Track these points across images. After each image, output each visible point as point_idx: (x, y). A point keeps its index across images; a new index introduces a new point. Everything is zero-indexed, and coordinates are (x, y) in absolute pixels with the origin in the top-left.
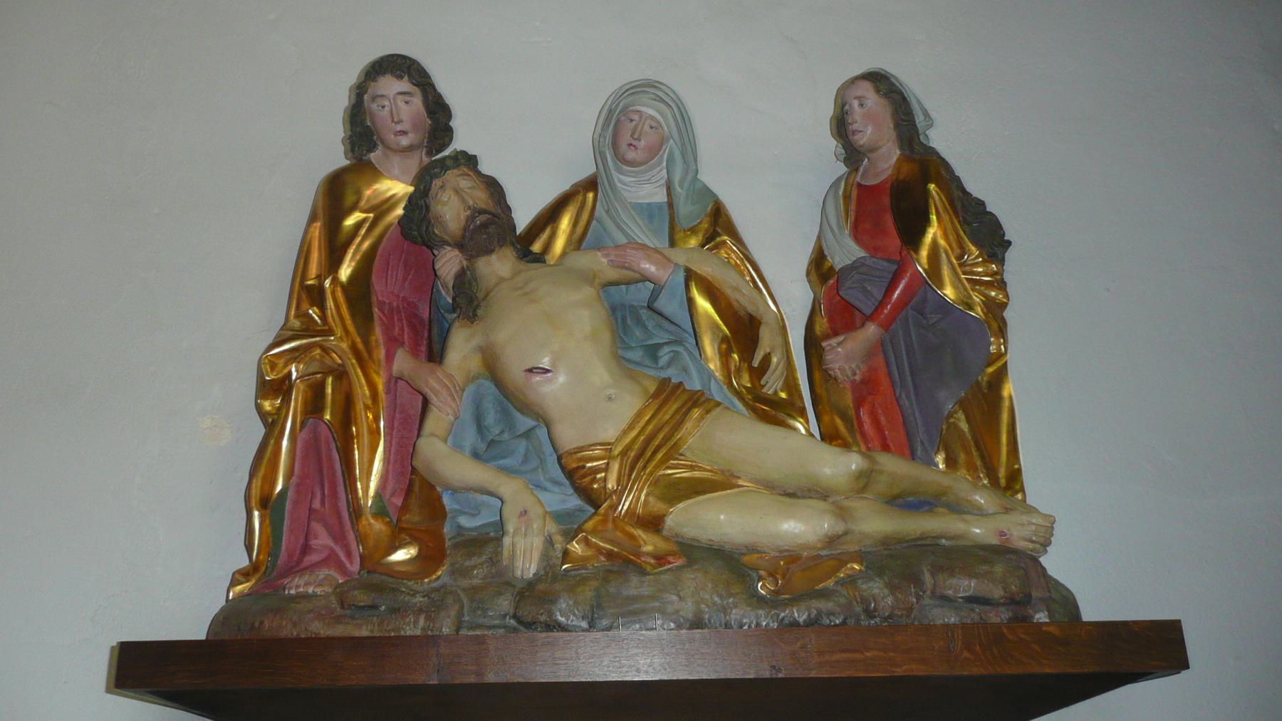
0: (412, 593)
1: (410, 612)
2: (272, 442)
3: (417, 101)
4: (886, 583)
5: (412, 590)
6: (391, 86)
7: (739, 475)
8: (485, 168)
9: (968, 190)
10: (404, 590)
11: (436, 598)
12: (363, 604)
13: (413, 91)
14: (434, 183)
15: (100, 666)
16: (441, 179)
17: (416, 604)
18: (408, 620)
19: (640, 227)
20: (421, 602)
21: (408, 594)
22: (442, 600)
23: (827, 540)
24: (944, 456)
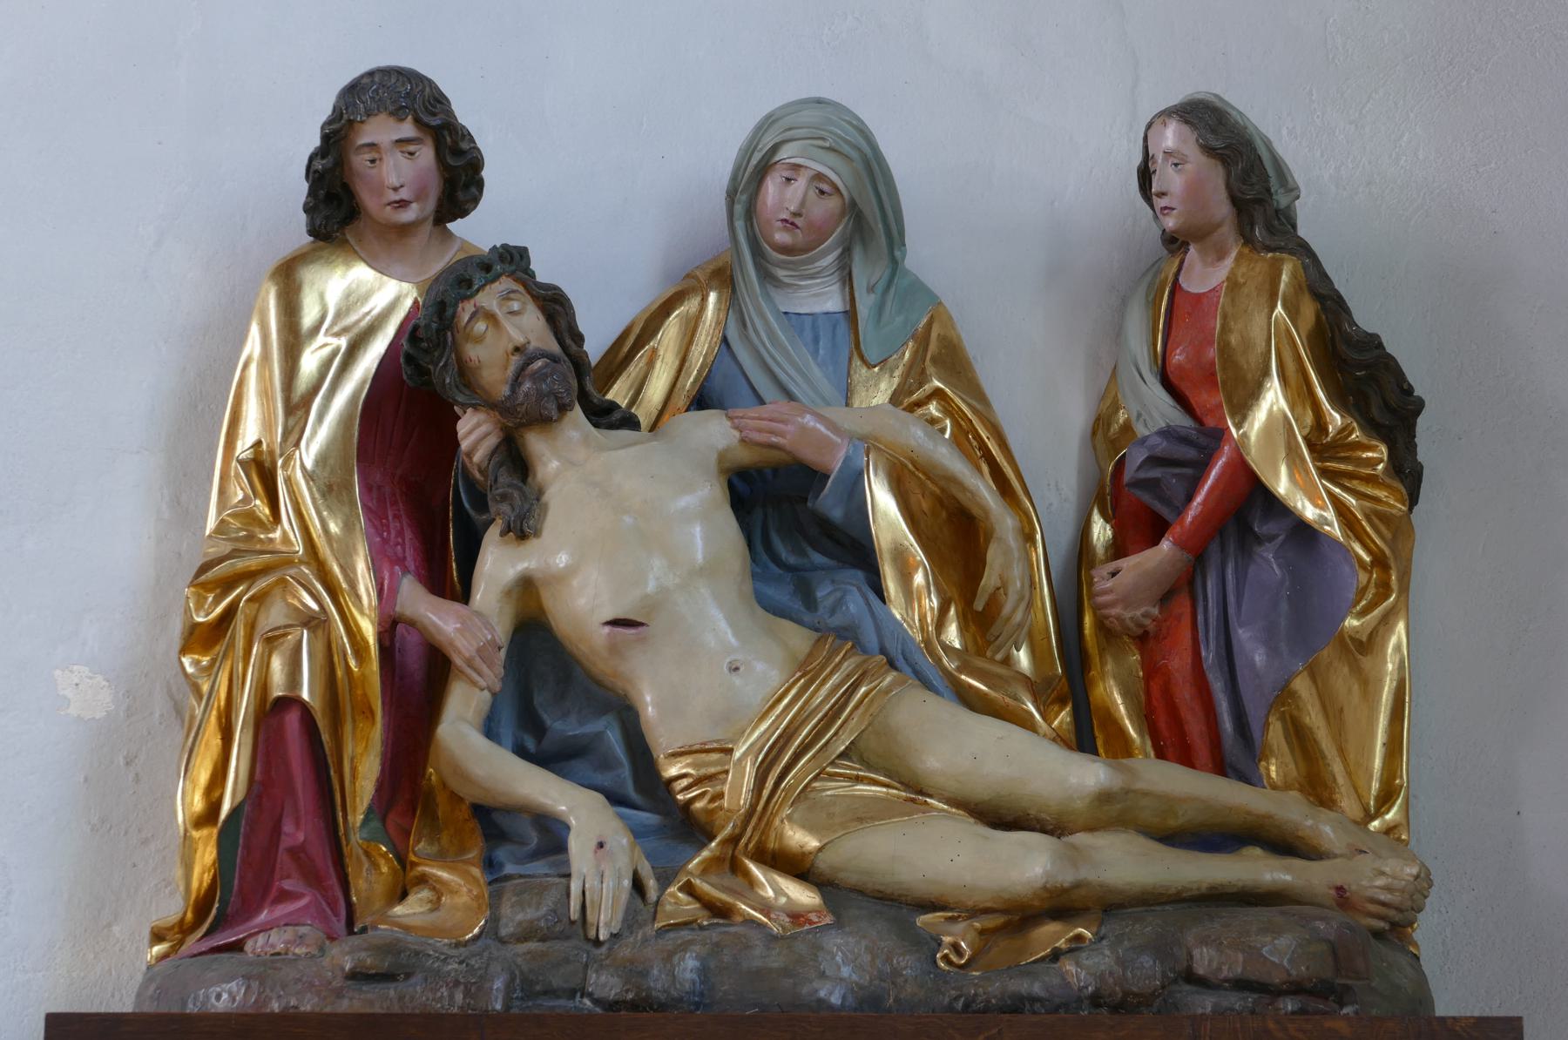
0: (443, 957)
1: (441, 983)
2: (707, 747)
3: (426, 155)
4: (1118, 958)
5: (442, 954)
6: (381, 131)
7: (931, 793)
8: (544, 270)
9: (1370, 331)
10: (431, 953)
11: (477, 966)
12: (374, 972)
13: (422, 137)
14: (460, 305)
15: (602, 840)
16: (472, 302)
17: (449, 973)
18: (439, 994)
19: (847, 833)
20: (456, 971)
21: (438, 958)
22: (486, 968)
23: (1046, 895)
24: (299, 713)
